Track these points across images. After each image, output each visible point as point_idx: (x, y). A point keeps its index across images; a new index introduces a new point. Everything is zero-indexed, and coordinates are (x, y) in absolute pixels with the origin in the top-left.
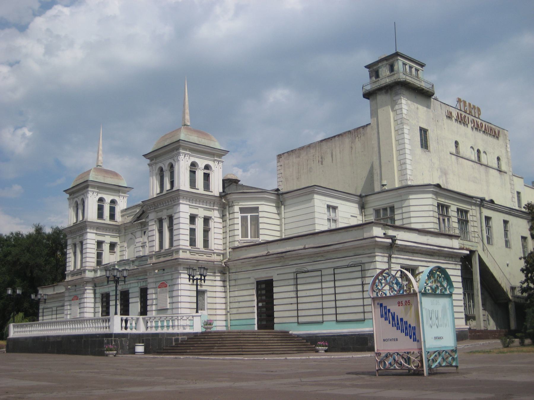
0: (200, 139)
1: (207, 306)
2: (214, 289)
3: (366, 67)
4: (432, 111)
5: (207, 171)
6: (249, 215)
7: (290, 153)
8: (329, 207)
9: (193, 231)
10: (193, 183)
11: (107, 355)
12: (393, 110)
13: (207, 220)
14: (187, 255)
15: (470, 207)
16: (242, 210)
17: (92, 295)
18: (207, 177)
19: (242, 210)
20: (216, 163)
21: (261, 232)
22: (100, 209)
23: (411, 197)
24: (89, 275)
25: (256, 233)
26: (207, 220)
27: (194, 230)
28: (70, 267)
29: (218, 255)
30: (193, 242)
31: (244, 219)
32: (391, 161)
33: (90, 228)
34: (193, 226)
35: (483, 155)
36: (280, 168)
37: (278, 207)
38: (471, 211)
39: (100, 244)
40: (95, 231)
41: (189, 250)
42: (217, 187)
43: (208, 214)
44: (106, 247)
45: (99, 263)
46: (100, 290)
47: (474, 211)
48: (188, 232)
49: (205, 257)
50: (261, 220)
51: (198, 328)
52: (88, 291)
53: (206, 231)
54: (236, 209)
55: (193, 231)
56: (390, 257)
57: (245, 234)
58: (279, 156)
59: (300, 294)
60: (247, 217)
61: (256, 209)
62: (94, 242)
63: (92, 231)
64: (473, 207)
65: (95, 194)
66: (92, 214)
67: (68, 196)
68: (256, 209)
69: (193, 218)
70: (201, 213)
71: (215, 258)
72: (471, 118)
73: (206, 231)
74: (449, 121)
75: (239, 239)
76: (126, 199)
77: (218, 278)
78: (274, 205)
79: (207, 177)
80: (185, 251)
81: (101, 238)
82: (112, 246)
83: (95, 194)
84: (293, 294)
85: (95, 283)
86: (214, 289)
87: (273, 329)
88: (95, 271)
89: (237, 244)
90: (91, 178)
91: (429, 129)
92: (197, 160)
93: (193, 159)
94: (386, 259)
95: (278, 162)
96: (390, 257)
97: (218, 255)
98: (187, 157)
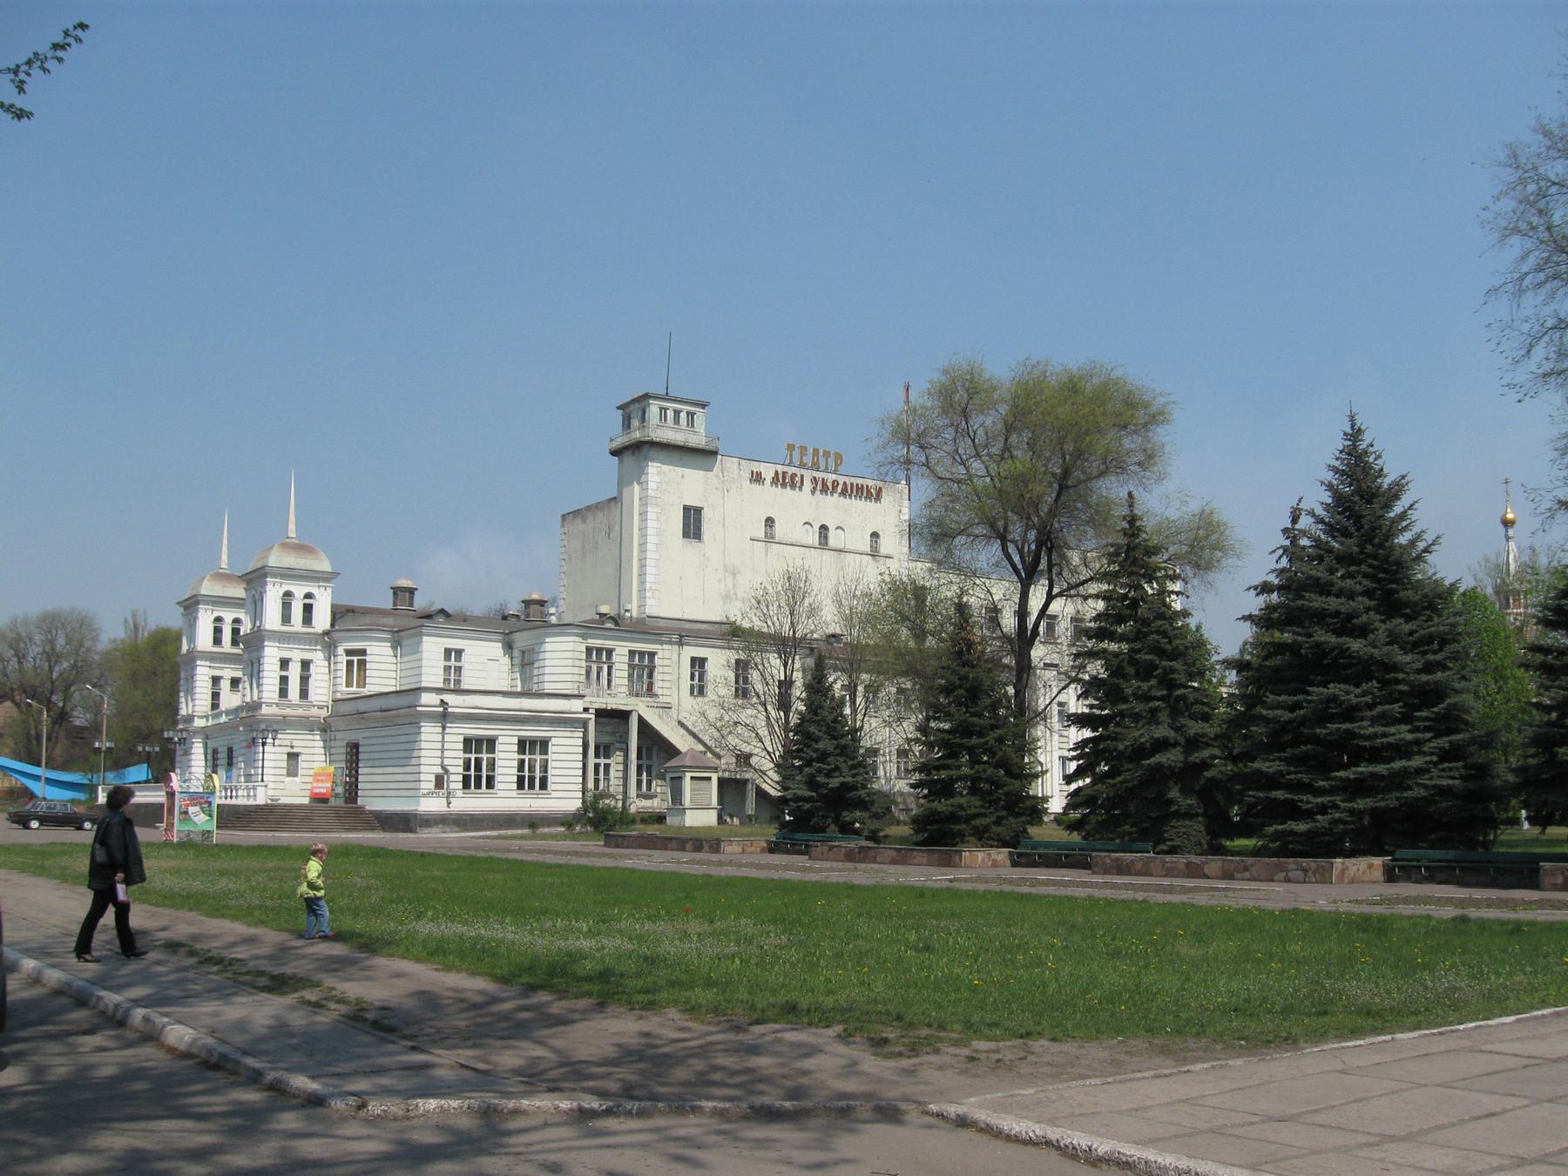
0: (299, 560)
1: (300, 772)
2: (312, 751)
3: (618, 408)
4: (717, 476)
5: (308, 601)
6: (355, 659)
7: (576, 513)
8: (448, 652)
9: (284, 680)
10: (286, 618)
11: (157, 828)
12: (639, 483)
13: (306, 665)
14: (274, 710)
15: (659, 647)
16: (349, 652)
17: (202, 751)
18: (308, 609)
19: (349, 652)
20: (322, 589)
21: (368, 680)
22: (218, 631)
23: (547, 640)
24: (199, 723)
25: (362, 684)
26: (306, 665)
27: (287, 677)
28: (183, 712)
29: (320, 707)
30: (283, 693)
31: (350, 664)
32: (631, 561)
33: (270, 640)
34: (284, 673)
35: (832, 534)
36: (564, 536)
37: (394, 648)
38: (660, 653)
39: (216, 680)
40: (277, 644)
41: (277, 704)
42: (322, 620)
43: (307, 656)
44: (225, 685)
45: (215, 706)
46: (211, 744)
47: (667, 654)
48: (277, 681)
49: (300, 712)
50: (368, 665)
51: (1537, 654)
52: (196, 745)
53: (305, 680)
54: (340, 650)
55: (284, 680)
56: (444, 728)
57: (349, 684)
58: (564, 517)
59: (447, 754)
60: (353, 661)
61: (363, 652)
62: (207, 678)
63: (271, 644)
64: (665, 646)
65: (209, 612)
66: (272, 618)
67: (182, 610)
68: (363, 652)
69: (284, 663)
70: (296, 655)
71: (314, 711)
72: (808, 475)
73: (305, 680)
74: (756, 487)
75: (343, 690)
76: (329, 590)
77: (318, 737)
78: (389, 644)
79: (308, 609)
80: (269, 705)
81: (217, 673)
82: (235, 682)
83: (277, 586)
84: (439, 753)
85: (206, 734)
86: (312, 751)
87: (356, 803)
88: (207, 717)
89: (339, 696)
90: (203, 592)
91: (705, 506)
92: (292, 589)
93: (285, 588)
94: (440, 730)
95: (563, 526)
96: (444, 728)
97: (320, 707)
98: (277, 586)
